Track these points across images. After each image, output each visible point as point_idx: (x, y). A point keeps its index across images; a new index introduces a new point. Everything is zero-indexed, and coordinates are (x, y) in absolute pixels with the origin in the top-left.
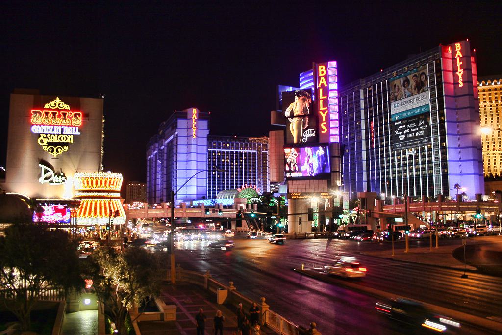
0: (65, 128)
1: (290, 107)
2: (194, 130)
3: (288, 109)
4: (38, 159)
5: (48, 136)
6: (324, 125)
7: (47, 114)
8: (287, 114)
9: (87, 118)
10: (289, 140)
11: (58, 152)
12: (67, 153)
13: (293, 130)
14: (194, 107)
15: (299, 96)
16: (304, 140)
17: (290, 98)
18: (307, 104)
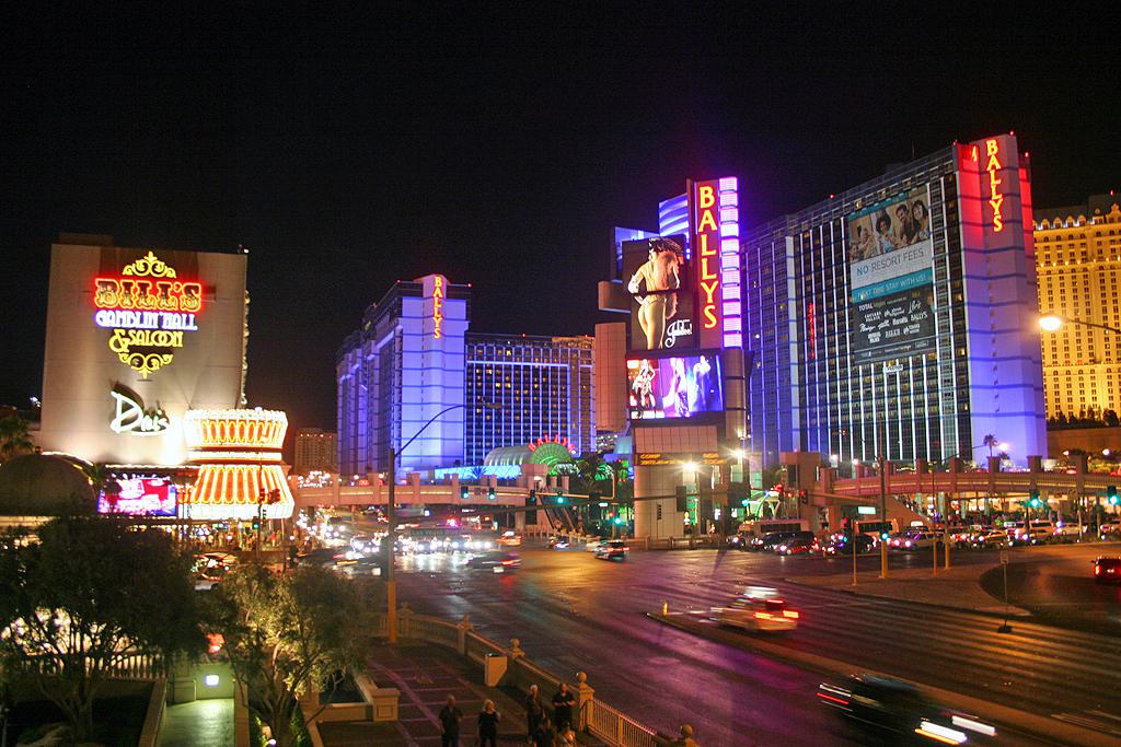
0: (167, 317)
1: (638, 273)
2: (438, 322)
3: (634, 278)
4: (110, 381)
5: (131, 333)
6: (710, 310)
7: (128, 286)
8: (633, 287)
10: (636, 343)
14: (437, 273)
15: (657, 251)
16: (669, 343)
18: (674, 267)
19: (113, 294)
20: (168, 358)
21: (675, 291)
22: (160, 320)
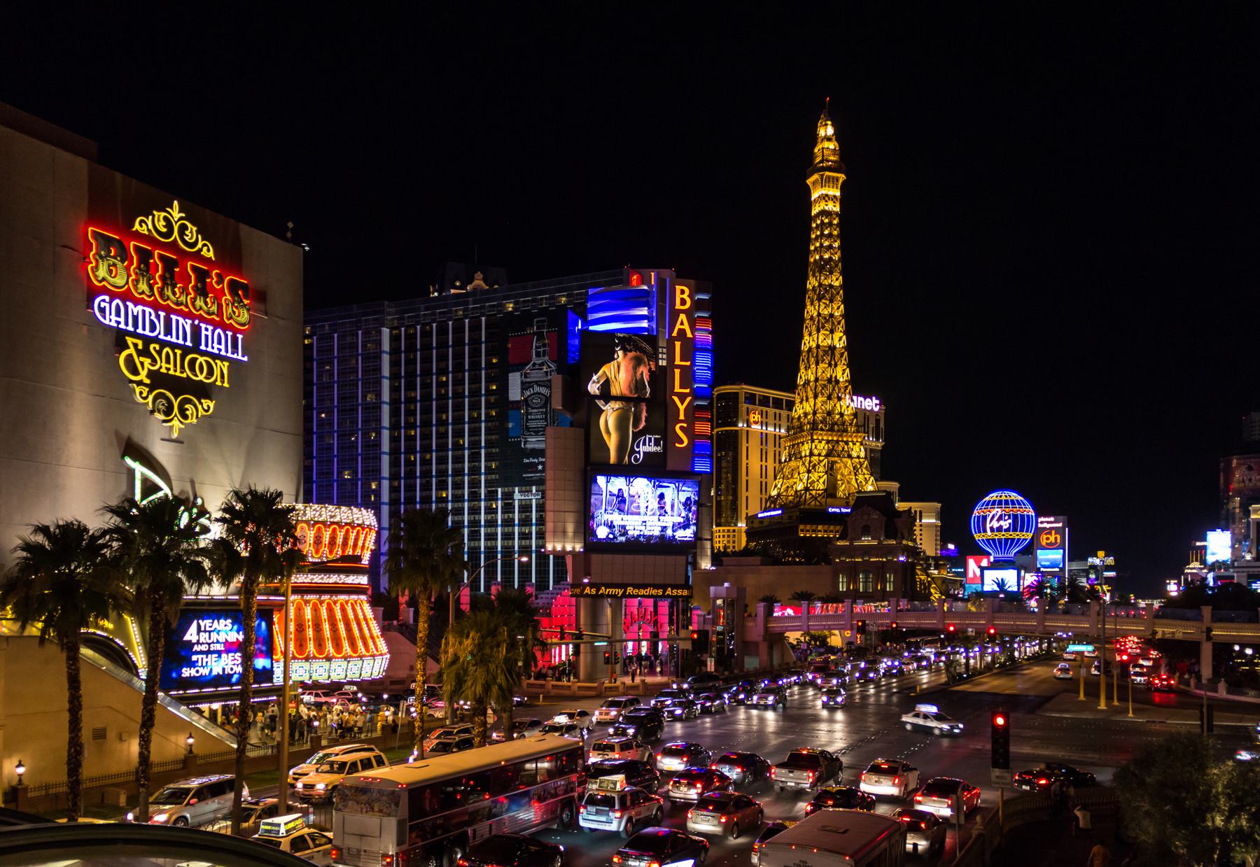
0: (206, 330)
1: (600, 373)
4: (117, 434)
5: (153, 347)
6: (681, 428)
7: (144, 256)
8: (593, 388)
9: (262, 307)
10: (596, 456)
11: (186, 417)
12: (208, 424)
13: (608, 432)
15: (625, 350)
16: (636, 460)
17: (603, 349)
18: (644, 371)
19: (119, 264)
20: (209, 404)
21: (645, 400)
22: (196, 331)
